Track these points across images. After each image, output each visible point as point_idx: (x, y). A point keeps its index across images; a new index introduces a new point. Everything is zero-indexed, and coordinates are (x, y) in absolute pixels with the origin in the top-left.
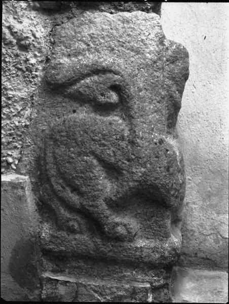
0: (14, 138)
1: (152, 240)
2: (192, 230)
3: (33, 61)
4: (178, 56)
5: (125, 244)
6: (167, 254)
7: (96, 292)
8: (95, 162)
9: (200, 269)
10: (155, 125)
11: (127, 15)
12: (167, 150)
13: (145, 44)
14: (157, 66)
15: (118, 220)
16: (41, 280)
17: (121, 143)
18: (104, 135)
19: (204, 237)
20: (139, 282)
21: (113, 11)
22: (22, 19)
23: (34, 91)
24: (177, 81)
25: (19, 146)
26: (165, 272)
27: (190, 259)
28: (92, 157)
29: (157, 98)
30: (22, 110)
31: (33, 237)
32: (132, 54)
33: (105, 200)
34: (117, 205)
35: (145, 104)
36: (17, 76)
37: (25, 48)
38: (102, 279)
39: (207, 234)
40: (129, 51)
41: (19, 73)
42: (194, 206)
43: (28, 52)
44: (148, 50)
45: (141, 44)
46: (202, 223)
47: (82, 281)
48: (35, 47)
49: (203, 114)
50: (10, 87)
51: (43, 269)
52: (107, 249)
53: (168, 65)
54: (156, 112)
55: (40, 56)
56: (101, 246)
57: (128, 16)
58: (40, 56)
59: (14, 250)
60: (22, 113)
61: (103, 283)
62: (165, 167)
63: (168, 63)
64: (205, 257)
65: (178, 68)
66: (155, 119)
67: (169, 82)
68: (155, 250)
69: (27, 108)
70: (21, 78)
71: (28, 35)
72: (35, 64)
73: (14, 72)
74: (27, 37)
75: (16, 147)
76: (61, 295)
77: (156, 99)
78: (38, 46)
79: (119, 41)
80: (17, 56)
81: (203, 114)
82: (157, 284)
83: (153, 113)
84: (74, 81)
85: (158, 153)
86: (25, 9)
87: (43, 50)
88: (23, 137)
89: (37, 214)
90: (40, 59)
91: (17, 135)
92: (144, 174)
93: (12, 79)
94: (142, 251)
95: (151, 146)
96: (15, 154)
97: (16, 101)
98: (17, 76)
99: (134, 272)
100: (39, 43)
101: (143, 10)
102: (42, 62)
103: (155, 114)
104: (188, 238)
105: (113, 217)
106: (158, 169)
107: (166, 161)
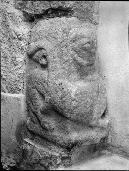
0: (20, 78)
1: (62, 133)
2: (116, 134)
3: (23, 45)
4: (76, 38)
5: (49, 132)
6: (66, 142)
7: (40, 152)
8: (36, 92)
9: (121, 157)
10: (62, 75)
11: (51, 20)
12: (63, 89)
13: (57, 34)
14: (62, 45)
15: (46, 120)
16: (23, 141)
17: (44, 84)
18: (39, 80)
19: (122, 139)
20: (56, 152)
21: (47, 18)
22: (19, 27)
23: (25, 58)
24: (77, 52)
25: (23, 82)
26: (67, 151)
27: (116, 149)
28: (36, 90)
29: (63, 61)
30: (22, 66)
31: (22, 122)
32: (53, 39)
33: (40, 110)
34: (45, 113)
35: (57, 65)
36: (19, 51)
37: (20, 39)
38: (45, 147)
39: (124, 137)
40: (52, 38)
41: (20, 50)
42: (118, 120)
43: (21, 41)
44: (58, 37)
45: (56, 34)
46: (122, 131)
47: (36, 146)
48: (24, 38)
49: (122, 67)
50: (17, 56)
51: (27, 137)
52: (44, 133)
53: (71, 43)
54: (62, 68)
55: (26, 42)
56: (42, 131)
57: (52, 20)
58: (26, 42)
59: (17, 126)
60: (22, 67)
61: (43, 149)
62: (60, 97)
63: (71, 42)
64: (123, 150)
65: (77, 44)
66: (62, 72)
67: (73, 52)
68: (61, 138)
69: (24, 65)
70: (20, 52)
71: (20, 33)
72: (24, 46)
73: (18, 50)
74: (20, 34)
75: (21, 82)
76: (28, 150)
77: (62, 62)
78: (24, 38)
79: (48, 33)
80: (17, 43)
81: (122, 67)
82: (64, 156)
83: (61, 69)
84: (34, 53)
85: (57, 90)
86: (21, 22)
87: (26, 39)
88: (24, 78)
89: (27, 113)
90: (26, 44)
91: (21, 77)
92: (50, 100)
93: (17, 53)
94: (56, 138)
95: (54, 86)
96: (21, 85)
97: (19, 63)
98: (19, 51)
99: (55, 147)
100: (25, 36)
101: (58, 17)
102: (27, 45)
103: (62, 69)
104: (115, 138)
105: (44, 118)
106: (56, 98)
107: (60, 94)
